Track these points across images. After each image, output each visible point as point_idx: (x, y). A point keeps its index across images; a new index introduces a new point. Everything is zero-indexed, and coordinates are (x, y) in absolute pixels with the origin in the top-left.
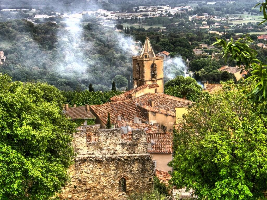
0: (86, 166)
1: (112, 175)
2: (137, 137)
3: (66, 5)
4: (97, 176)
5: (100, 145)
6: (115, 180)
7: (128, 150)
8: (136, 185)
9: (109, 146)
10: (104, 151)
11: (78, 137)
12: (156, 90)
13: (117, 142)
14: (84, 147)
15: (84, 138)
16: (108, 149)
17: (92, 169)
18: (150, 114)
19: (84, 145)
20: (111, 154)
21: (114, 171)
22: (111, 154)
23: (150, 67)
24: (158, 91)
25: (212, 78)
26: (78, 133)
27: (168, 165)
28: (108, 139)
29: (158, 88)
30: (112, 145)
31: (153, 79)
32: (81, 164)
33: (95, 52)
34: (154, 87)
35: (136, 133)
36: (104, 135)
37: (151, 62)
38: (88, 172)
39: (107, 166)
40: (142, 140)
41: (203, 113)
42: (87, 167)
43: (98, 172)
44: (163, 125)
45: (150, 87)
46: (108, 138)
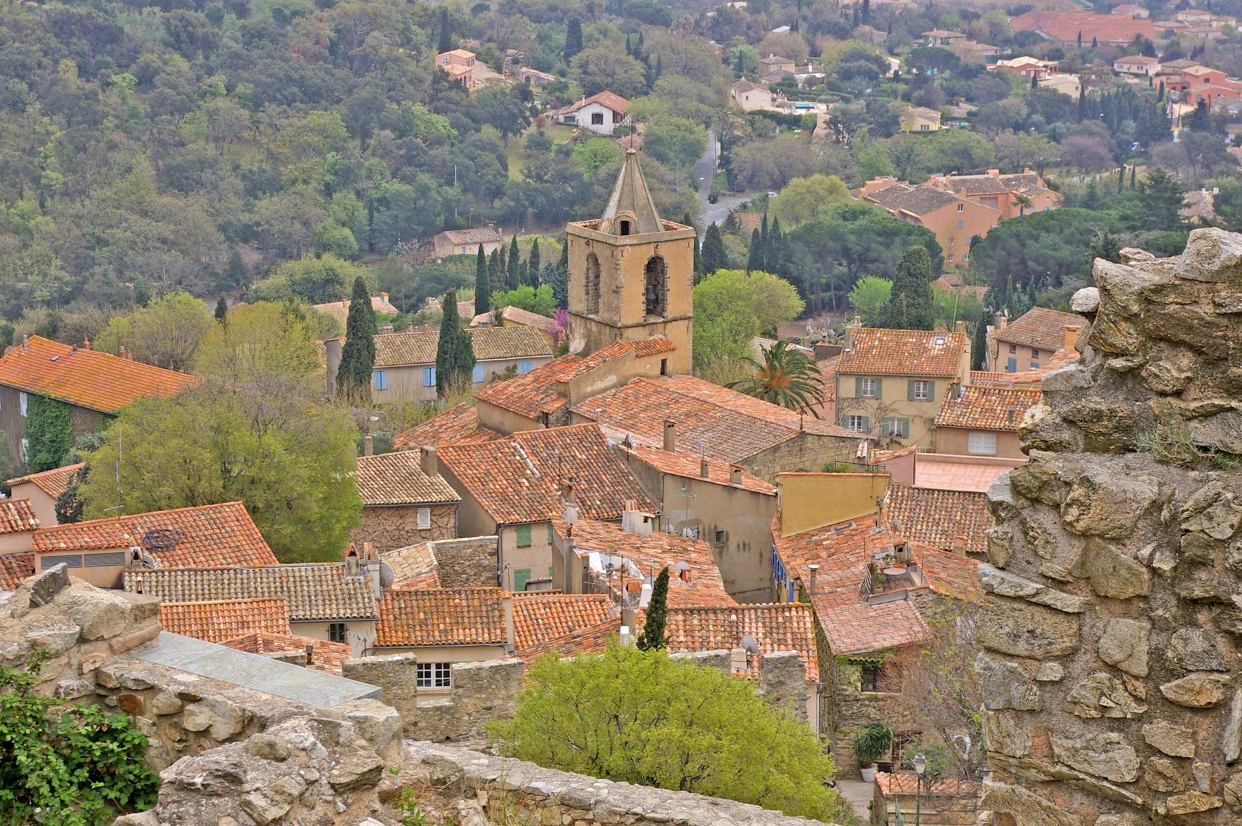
2: (777, 680)
12: (664, 362)
23: (642, 270)
24: (670, 367)
25: (839, 248)
29: (670, 357)
31: (652, 320)
33: (293, 94)
34: (659, 352)
35: (776, 667)
37: (650, 252)
40: (793, 688)
44: (716, 527)
45: (645, 350)
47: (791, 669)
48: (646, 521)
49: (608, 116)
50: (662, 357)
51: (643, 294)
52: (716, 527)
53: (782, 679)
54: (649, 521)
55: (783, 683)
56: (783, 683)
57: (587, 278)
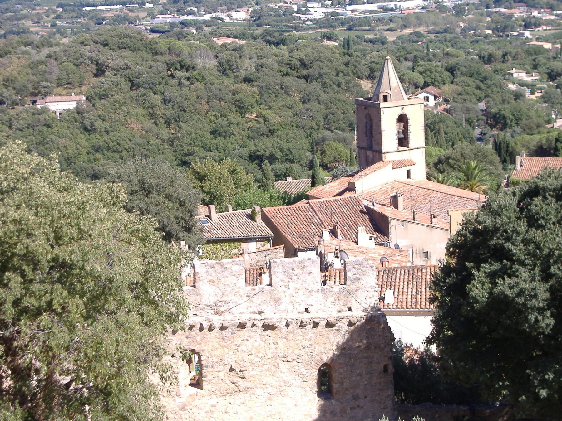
0: (246, 338)
1: (303, 358)
2: (355, 276)
3: (352, 23)
4: (270, 360)
5: (276, 292)
6: (309, 368)
7: (337, 302)
8: (354, 378)
9: (295, 295)
10: (283, 307)
11: (227, 277)
12: (409, 171)
13: (312, 285)
14: (239, 297)
15: (240, 277)
16: (292, 302)
17: (259, 345)
18: (392, 223)
19: (241, 294)
20: (299, 313)
21: (307, 349)
22: (299, 313)
26: (226, 268)
27: (191, 385)
28: (291, 279)
30: (301, 292)
32: (234, 333)
34: (406, 166)
36: (284, 272)
37: (398, 112)
38: (250, 351)
39: (290, 338)
41: (122, 231)
42: (247, 340)
43: (271, 351)
44: (423, 249)
45: (397, 165)
46: (293, 277)
47: (364, 269)
48: (371, 239)
49: (432, 98)
50: (408, 168)
51: (397, 135)
52: (423, 249)
53: (358, 276)
54: (373, 238)
55: (359, 279)
56: (359, 279)
57: (366, 128)
